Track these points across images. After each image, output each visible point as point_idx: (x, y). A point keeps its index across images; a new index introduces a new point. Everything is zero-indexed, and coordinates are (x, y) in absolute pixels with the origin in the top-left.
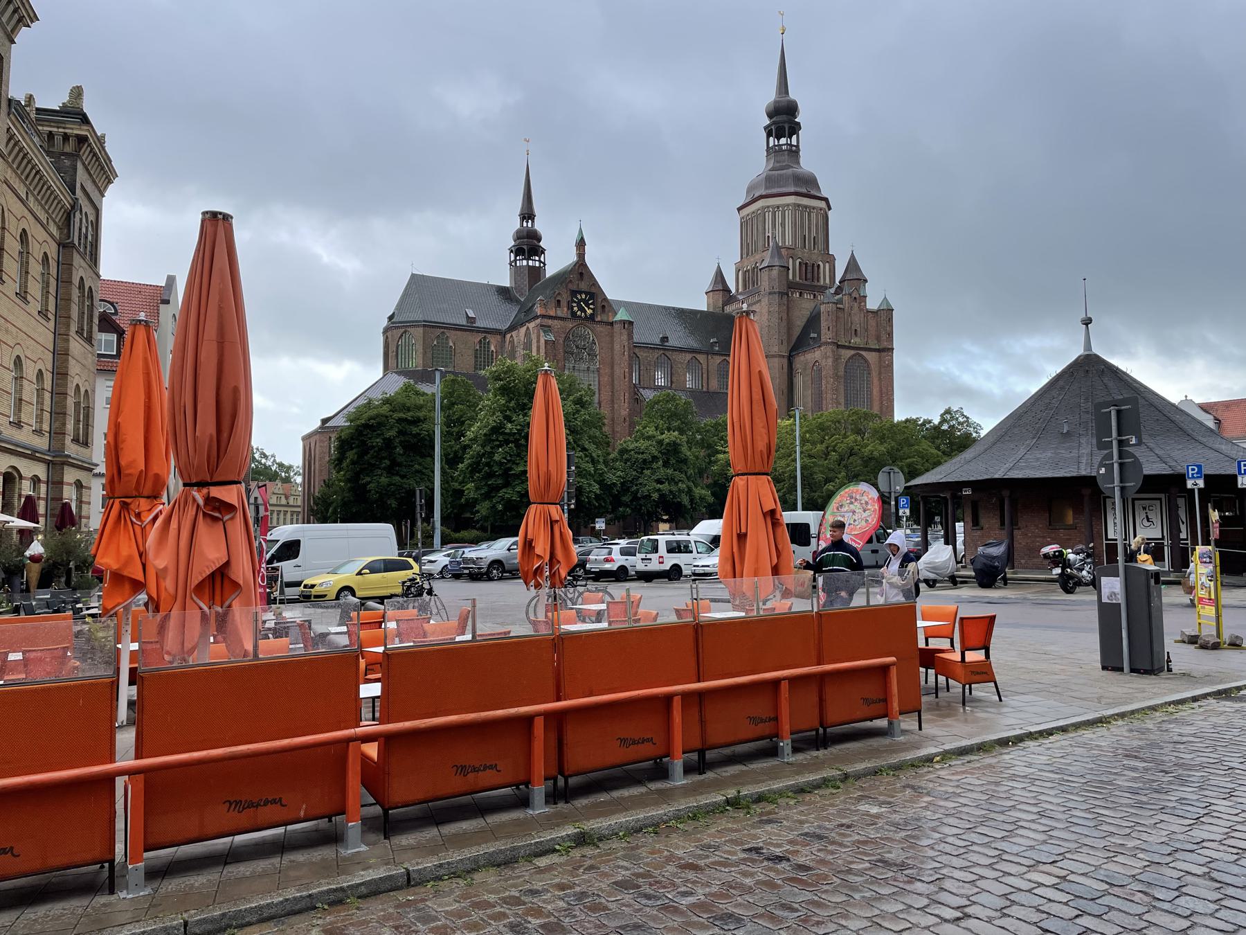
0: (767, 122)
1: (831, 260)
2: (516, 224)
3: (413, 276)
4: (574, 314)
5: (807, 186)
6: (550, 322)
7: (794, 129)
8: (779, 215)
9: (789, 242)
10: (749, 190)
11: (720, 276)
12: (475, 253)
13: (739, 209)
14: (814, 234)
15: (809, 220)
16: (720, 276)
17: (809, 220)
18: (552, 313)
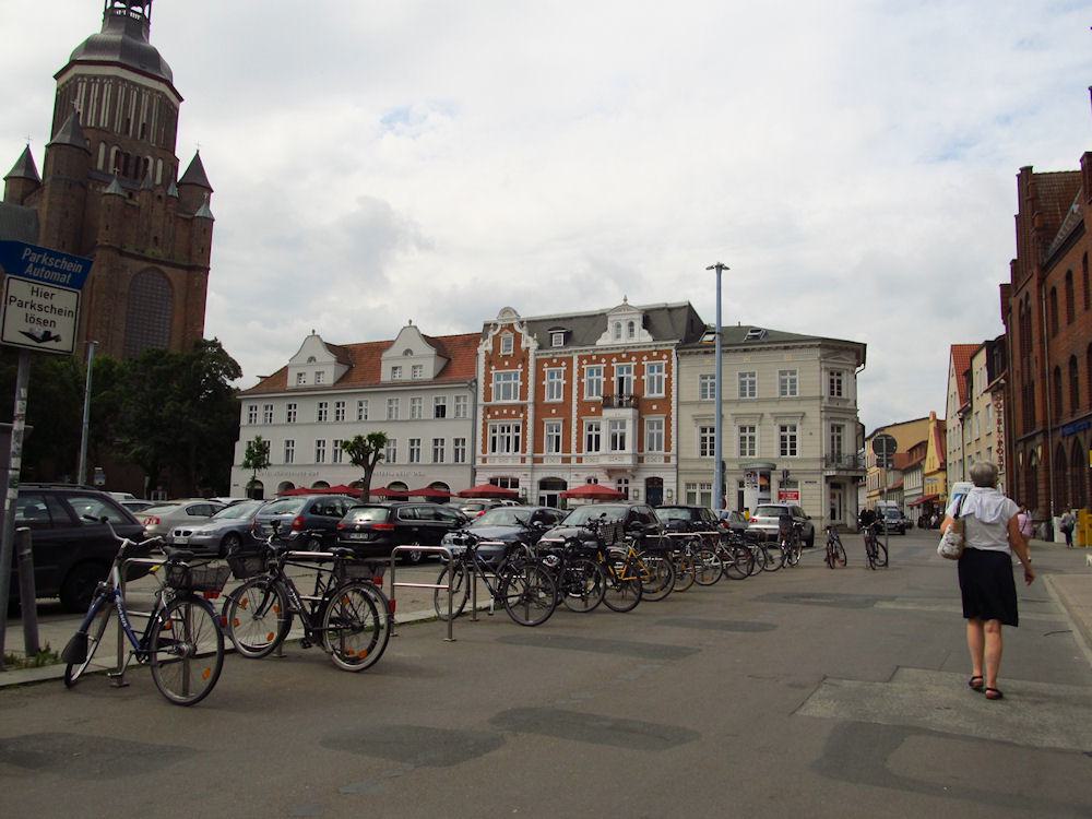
5: (151, 63)
8: (95, 89)
9: (104, 122)
11: (27, 158)
13: (57, 77)
16: (27, 158)
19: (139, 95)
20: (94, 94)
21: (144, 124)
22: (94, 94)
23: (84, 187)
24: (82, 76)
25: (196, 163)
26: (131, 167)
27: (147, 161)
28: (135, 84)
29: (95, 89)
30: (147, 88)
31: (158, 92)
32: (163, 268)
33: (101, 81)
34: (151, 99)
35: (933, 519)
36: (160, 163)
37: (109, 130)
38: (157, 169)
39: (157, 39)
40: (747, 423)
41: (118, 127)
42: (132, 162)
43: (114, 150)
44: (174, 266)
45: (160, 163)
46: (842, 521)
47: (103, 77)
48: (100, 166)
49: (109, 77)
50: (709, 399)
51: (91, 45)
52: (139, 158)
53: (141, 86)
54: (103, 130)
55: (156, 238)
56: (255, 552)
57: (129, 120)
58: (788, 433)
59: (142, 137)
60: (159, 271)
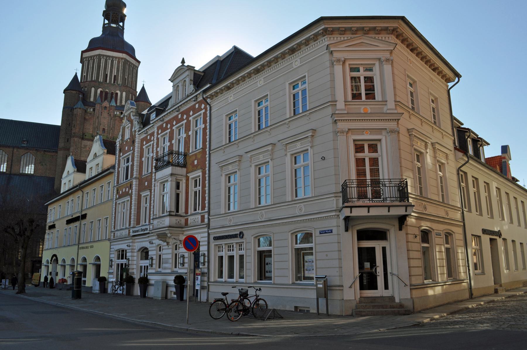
3: (235, 48)
14: (115, 73)
21: (115, 76)
25: (143, 89)
27: (117, 94)
29: (103, 61)
30: (116, 58)
31: (122, 59)
33: (106, 58)
34: (119, 62)
36: (124, 94)
39: (128, 37)
40: (364, 106)
41: (101, 79)
43: (99, 91)
45: (124, 94)
46: (387, 293)
48: (92, 99)
50: (197, 211)
52: (112, 93)
53: (113, 57)
54: (94, 81)
55: (104, 129)
57: (107, 75)
58: (362, 74)
59: (114, 82)
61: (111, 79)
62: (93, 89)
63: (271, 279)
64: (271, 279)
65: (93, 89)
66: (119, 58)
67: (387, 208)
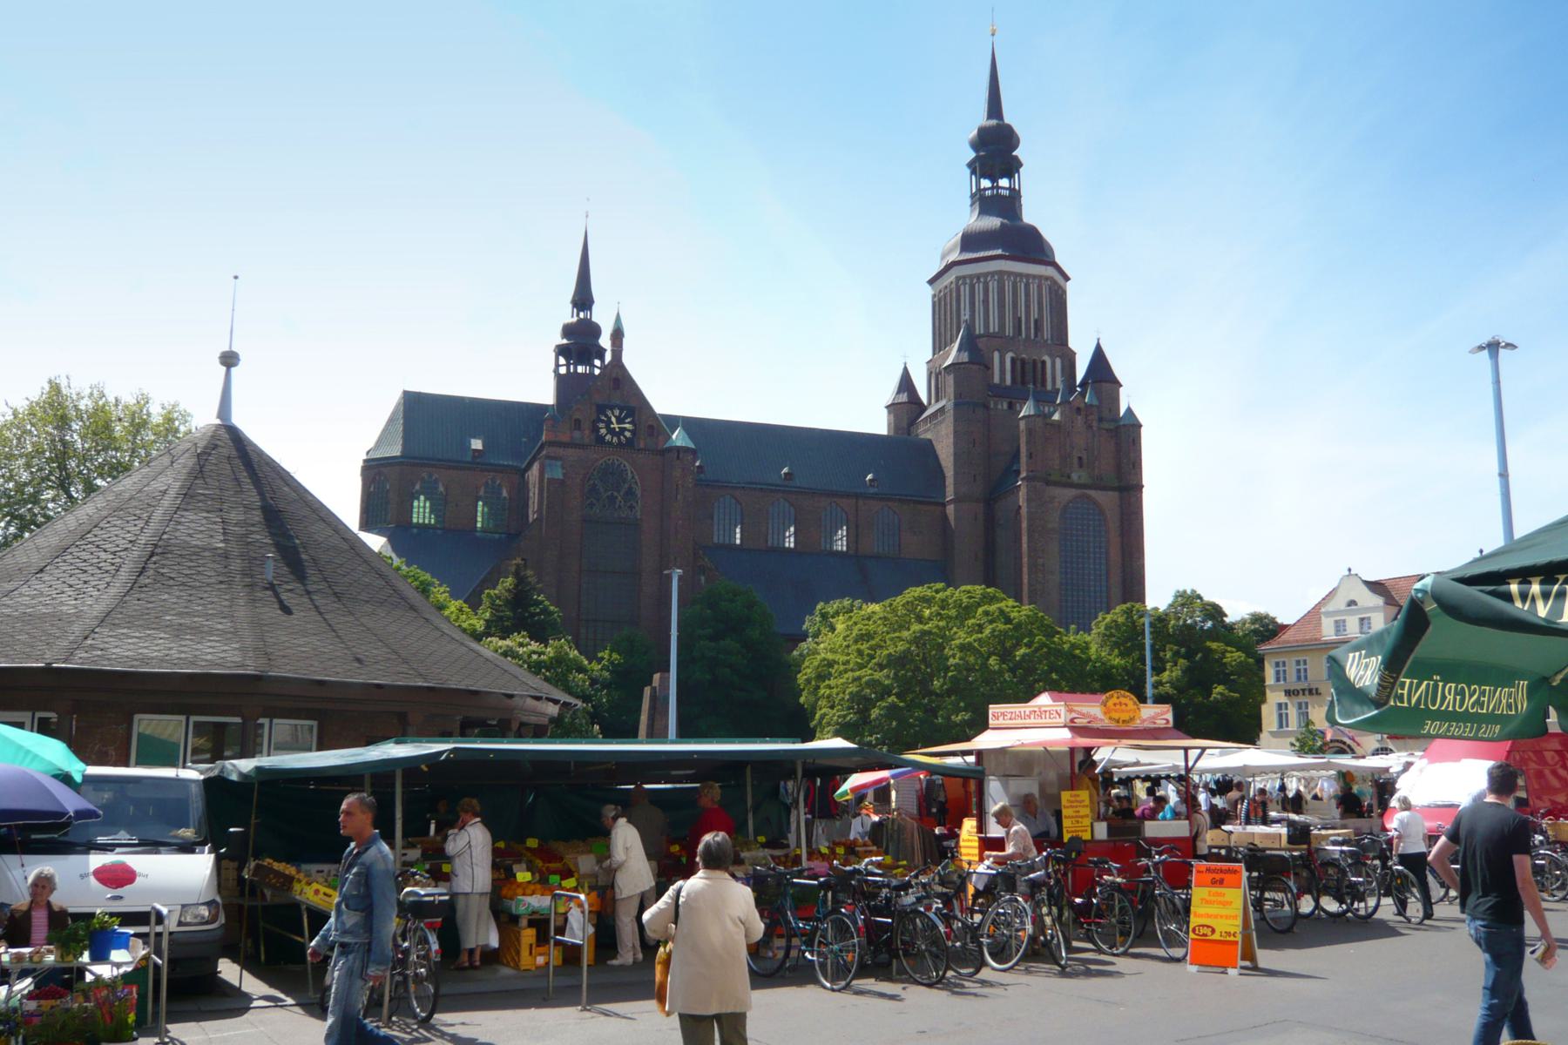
0: (972, 155)
1: (1069, 359)
2: (567, 315)
3: (406, 393)
4: (600, 440)
5: (1030, 246)
6: (560, 451)
7: (1011, 167)
8: (979, 288)
9: (994, 327)
10: (943, 257)
11: (906, 383)
12: (791, 335)
13: (931, 282)
14: (1034, 315)
15: (1027, 295)
16: (906, 383)
17: (1027, 295)
18: (565, 438)
19: (1027, 286)
20: (979, 296)
21: (1036, 321)
22: (979, 296)
23: (986, 407)
24: (964, 277)
26: (1029, 377)
27: (1044, 363)
28: (1021, 275)
29: (979, 288)
30: (1034, 277)
31: (1047, 278)
32: (1092, 493)
34: (1040, 287)
35: (421, 511)
36: (1058, 361)
37: (1000, 335)
38: (1053, 367)
41: (1009, 331)
42: (1029, 368)
44: (1104, 489)
47: (986, 275)
48: (997, 380)
49: (993, 274)
51: (970, 241)
53: (1028, 276)
56: (1093, 967)
60: (1088, 497)
61: (1028, 328)
62: (996, 355)
63: (197, 724)
64: (197, 724)
65: (996, 355)
66: (1040, 277)
67: (1182, 752)
